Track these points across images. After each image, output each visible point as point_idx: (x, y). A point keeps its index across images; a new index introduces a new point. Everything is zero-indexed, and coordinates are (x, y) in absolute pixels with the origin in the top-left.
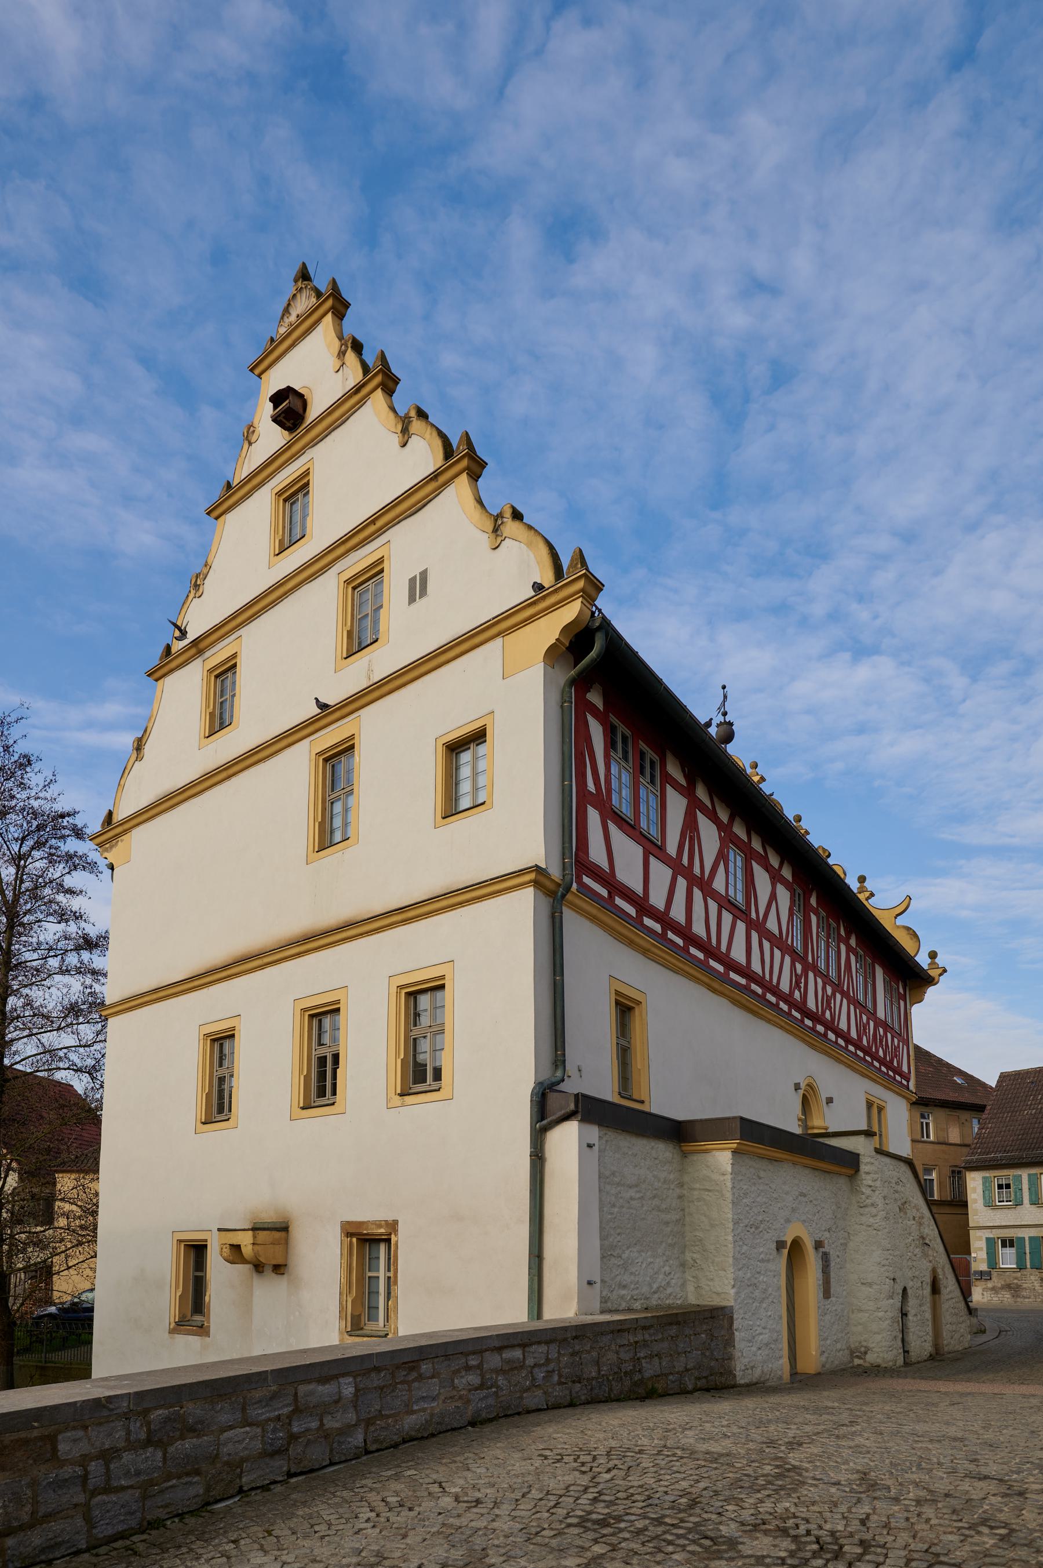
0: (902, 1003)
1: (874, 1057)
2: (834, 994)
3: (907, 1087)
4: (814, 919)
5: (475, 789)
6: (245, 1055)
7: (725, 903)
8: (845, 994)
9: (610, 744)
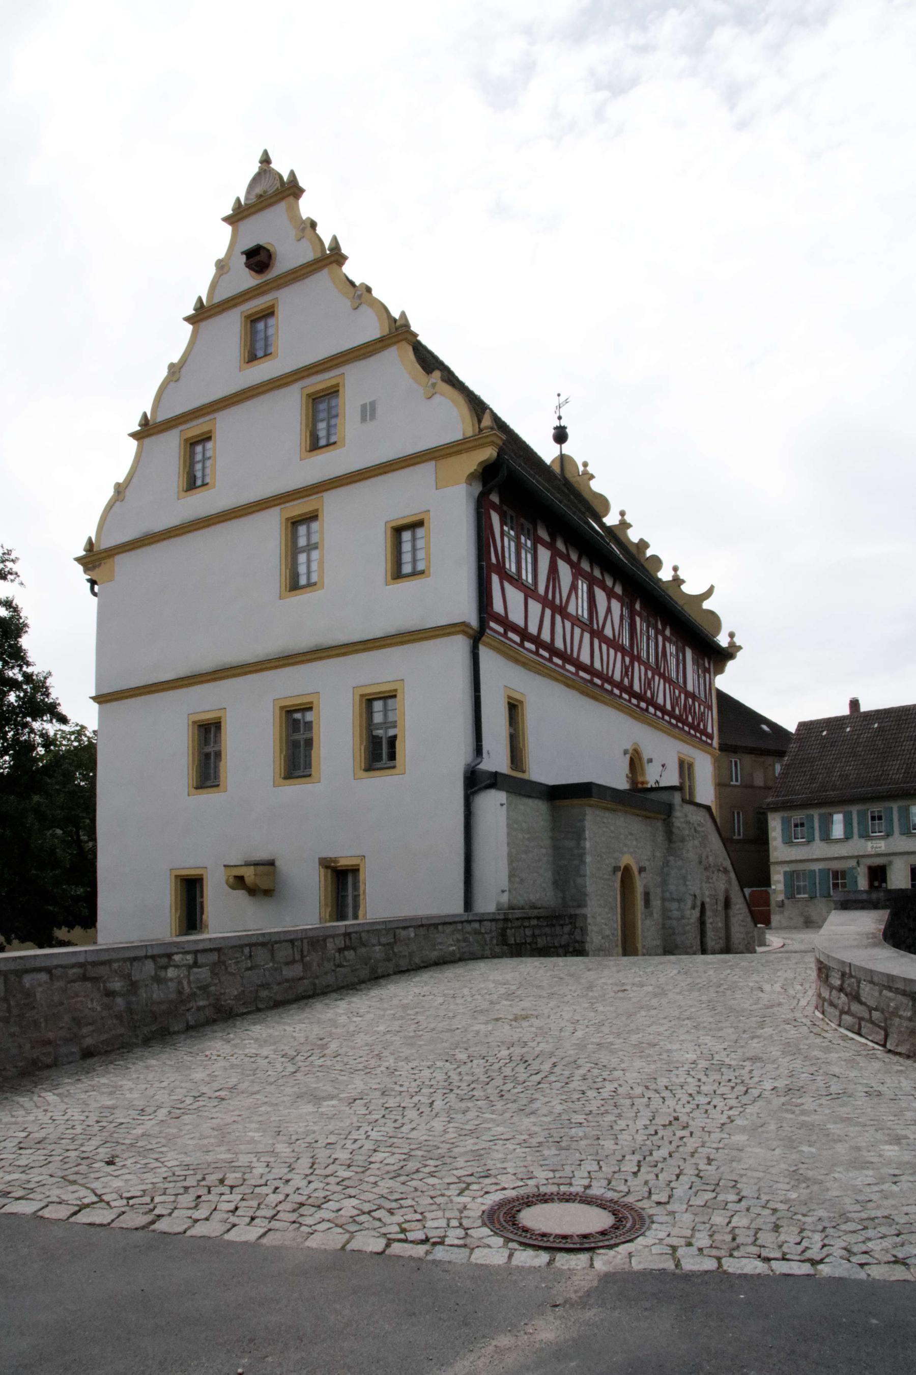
0: (707, 675)
1: (685, 723)
2: (653, 677)
3: (711, 745)
4: (638, 619)
5: (414, 561)
6: (232, 742)
7: (576, 621)
8: (662, 676)
9: (503, 523)
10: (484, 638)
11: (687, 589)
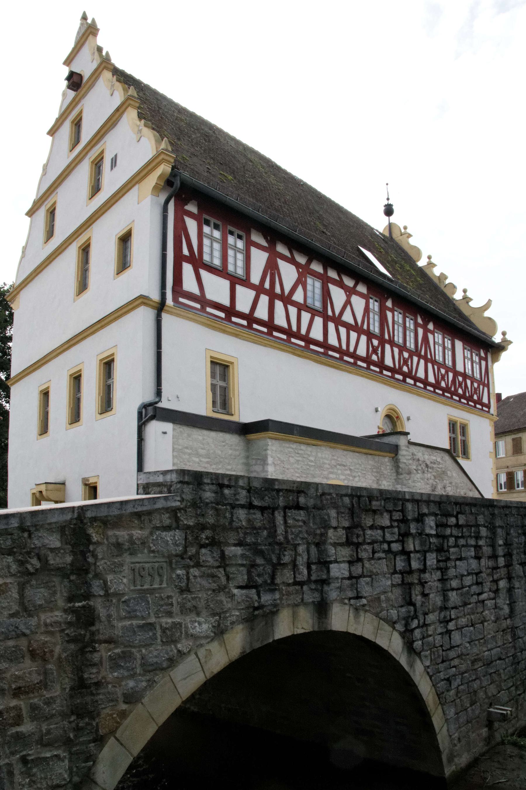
10: (165, 308)
11: (472, 304)
